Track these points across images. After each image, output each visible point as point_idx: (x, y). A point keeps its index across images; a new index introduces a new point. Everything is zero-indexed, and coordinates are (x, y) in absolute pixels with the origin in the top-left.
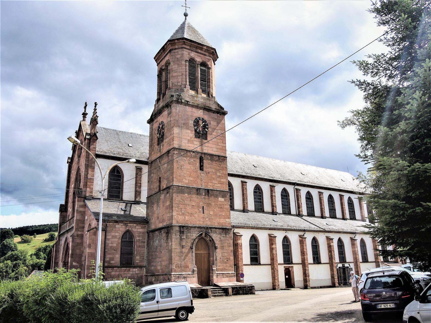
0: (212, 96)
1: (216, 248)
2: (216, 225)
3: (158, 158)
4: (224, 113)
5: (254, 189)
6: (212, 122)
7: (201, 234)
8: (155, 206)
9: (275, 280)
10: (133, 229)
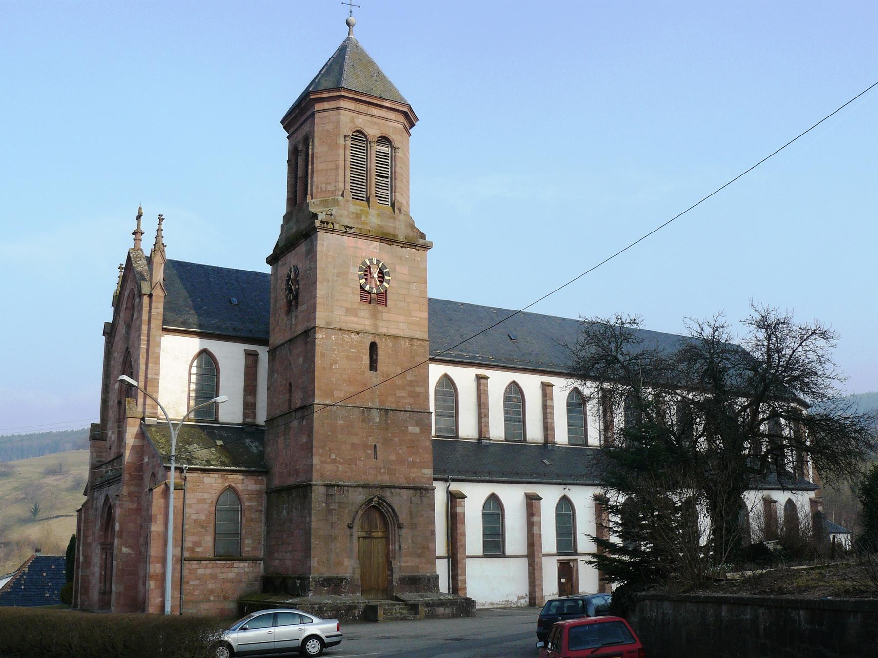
0: (399, 209)
1: (400, 527)
2: (403, 482)
3: (286, 342)
4: (426, 247)
6: (398, 268)
7: (371, 500)
8: (281, 440)
9: (534, 586)
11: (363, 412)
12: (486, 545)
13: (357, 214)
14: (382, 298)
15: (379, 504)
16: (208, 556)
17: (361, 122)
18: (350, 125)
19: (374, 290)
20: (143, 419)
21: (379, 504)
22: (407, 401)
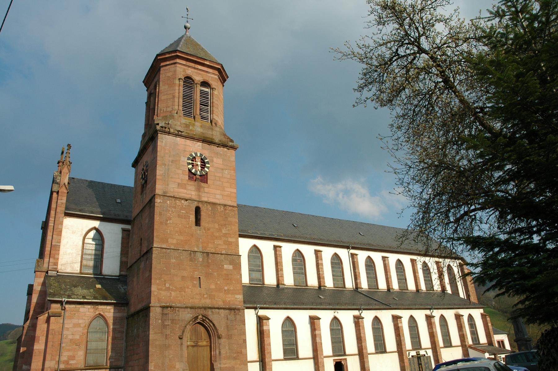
1: (219, 337)
2: (221, 304)
5: (293, 256)
6: (215, 159)
10: (106, 314)
11: (190, 254)
12: (285, 352)
13: (186, 125)
14: (204, 178)
15: (203, 320)
16: (79, 366)
17: (190, 72)
18: (182, 73)
19: (198, 173)
20: (47, 272)
21: (203, 320)
22: (224, 247)
